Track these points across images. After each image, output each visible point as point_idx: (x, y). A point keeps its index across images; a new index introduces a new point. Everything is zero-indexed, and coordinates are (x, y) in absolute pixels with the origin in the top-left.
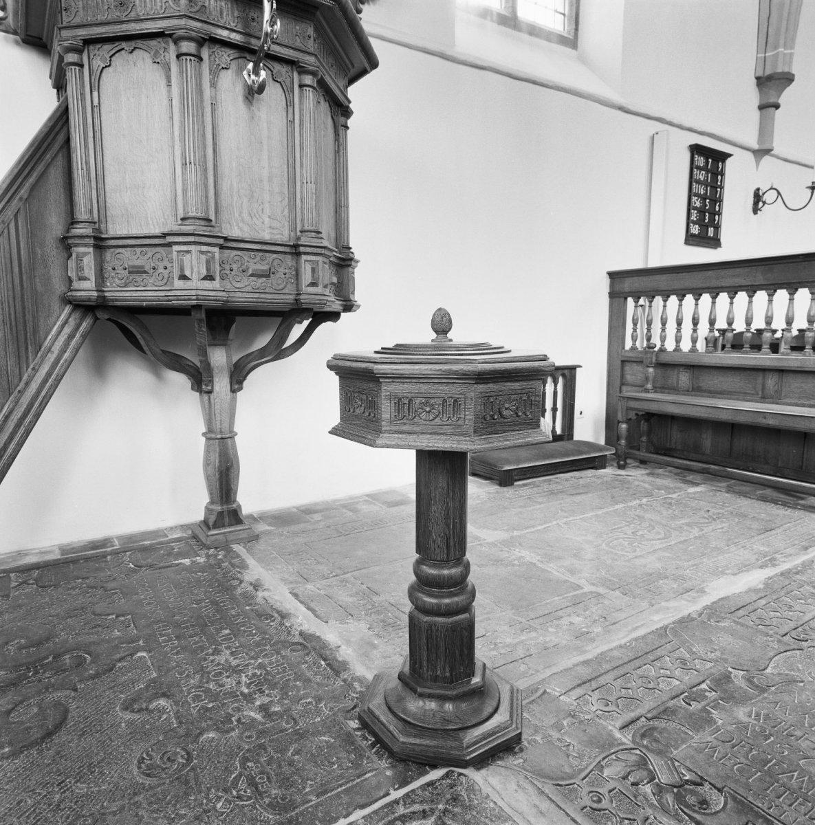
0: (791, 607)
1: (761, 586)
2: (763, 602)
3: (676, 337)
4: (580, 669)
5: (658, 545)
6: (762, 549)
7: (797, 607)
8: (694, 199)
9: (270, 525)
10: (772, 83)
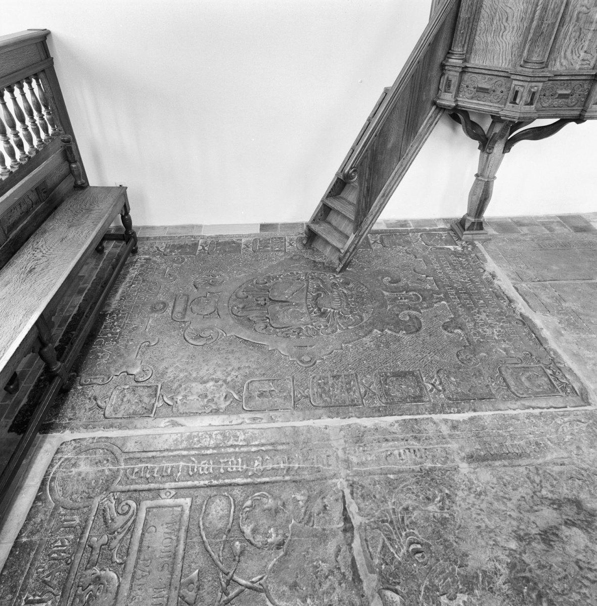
9: (495, 230)
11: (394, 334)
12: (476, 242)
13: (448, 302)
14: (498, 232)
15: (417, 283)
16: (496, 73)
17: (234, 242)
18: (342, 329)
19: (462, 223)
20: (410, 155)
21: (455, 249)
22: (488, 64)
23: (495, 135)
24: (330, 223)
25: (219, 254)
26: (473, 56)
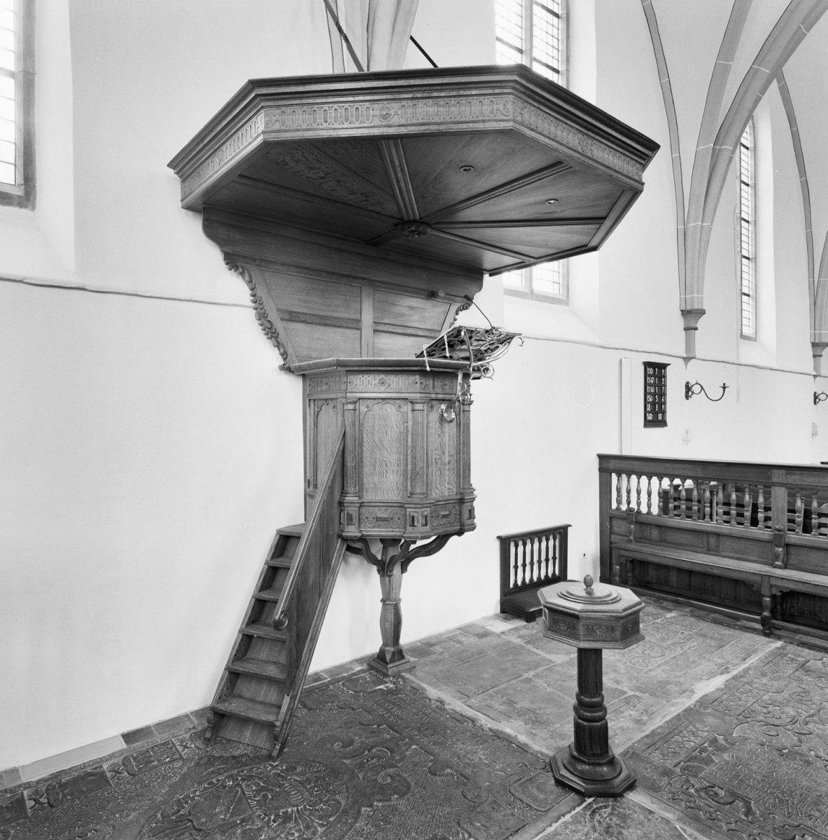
0: (740, 699)
1: (723, 687)
2: (725, 696)
3: (648, 504)
4: (646, 740)
5: (660, 661)
6: (720, 661)
7: (743, 698)
8: (648, 396)
10: (691, 315)
11: (386, 803)
12: (403, 674)
13: (418, 745)
14: (415, 657)
15: (373, 737)
16: (390, 505)
17: (91, 774)
18: (322, 825)
19: (381, 657)
20: (328, 589)
21: (387, 687)
22: (380, 498)
23: (392, 558)
24: (240, 697)
25: (73, 800)
26: (365, 493)
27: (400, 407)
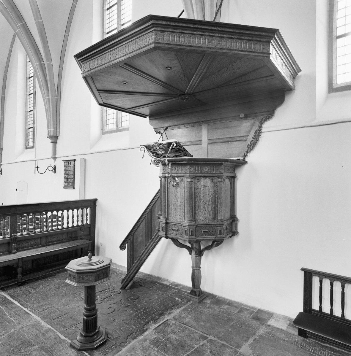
27: (212, 180)
